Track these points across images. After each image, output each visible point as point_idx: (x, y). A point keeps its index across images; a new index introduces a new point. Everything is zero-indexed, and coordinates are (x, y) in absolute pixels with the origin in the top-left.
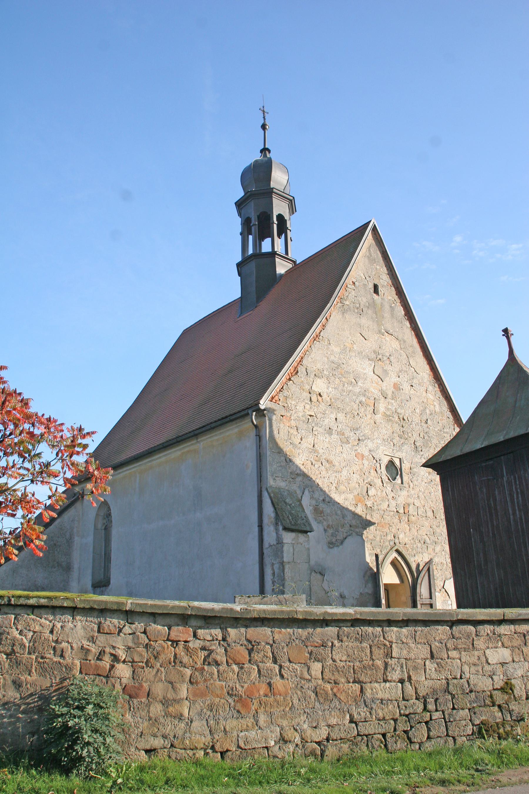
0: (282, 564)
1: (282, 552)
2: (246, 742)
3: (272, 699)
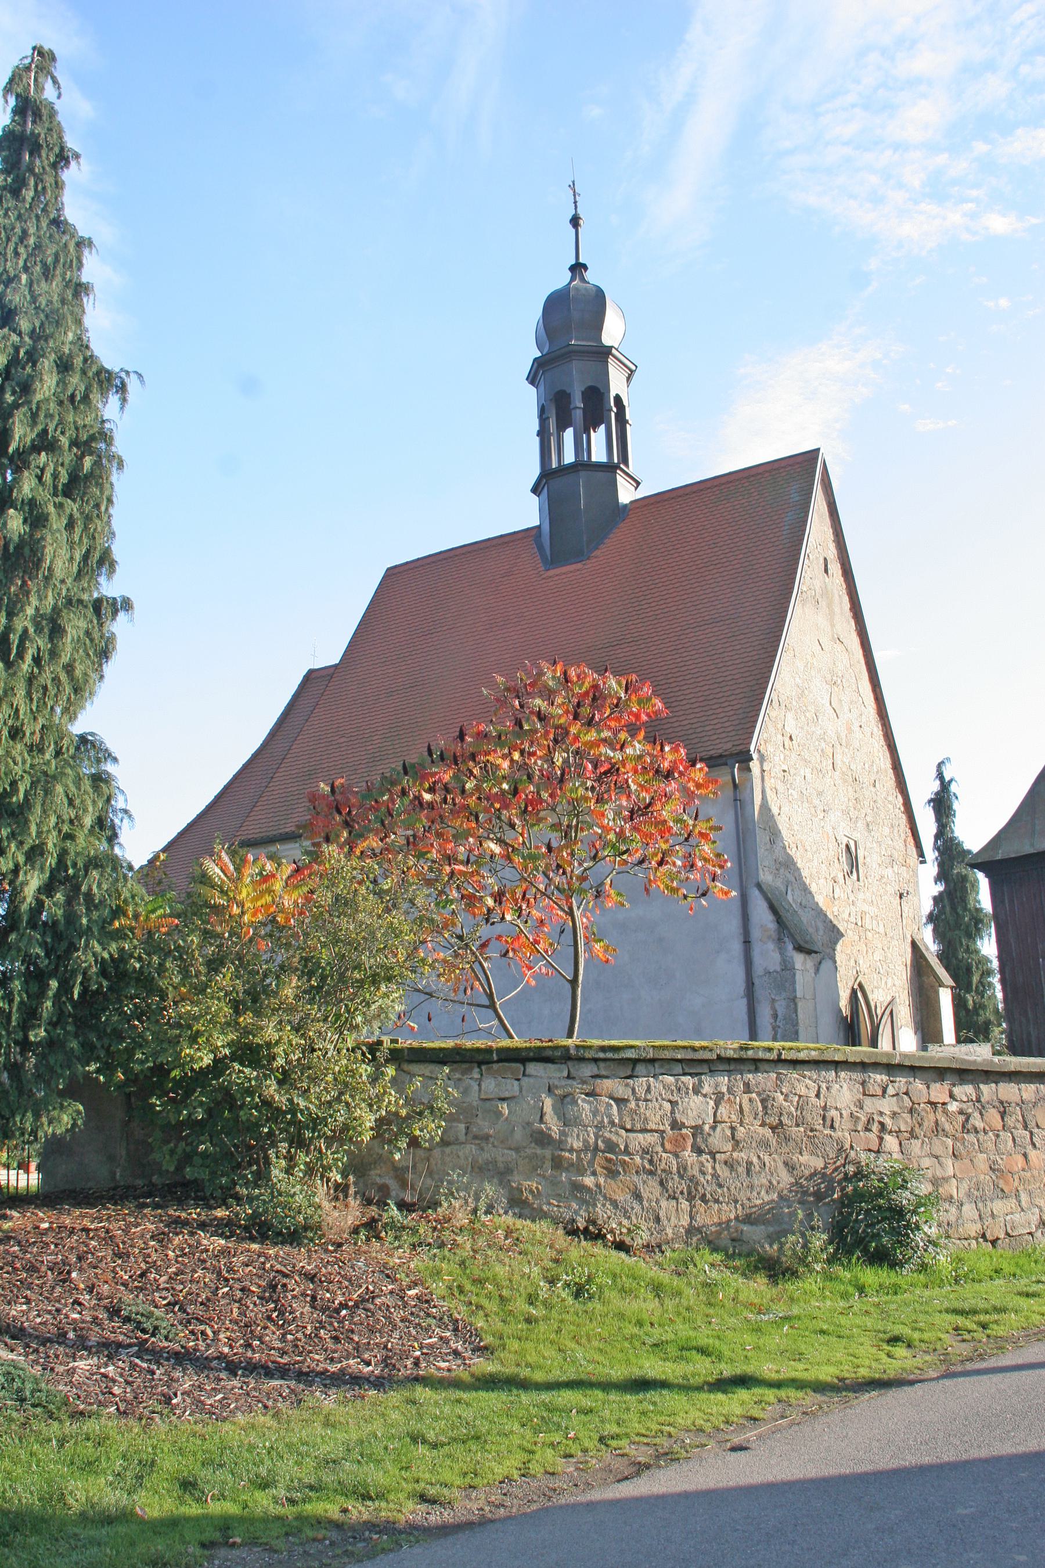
0: (793, 1000)
1: (794, 983)
2: (1013, 1228)
3: (1028, 1174)
